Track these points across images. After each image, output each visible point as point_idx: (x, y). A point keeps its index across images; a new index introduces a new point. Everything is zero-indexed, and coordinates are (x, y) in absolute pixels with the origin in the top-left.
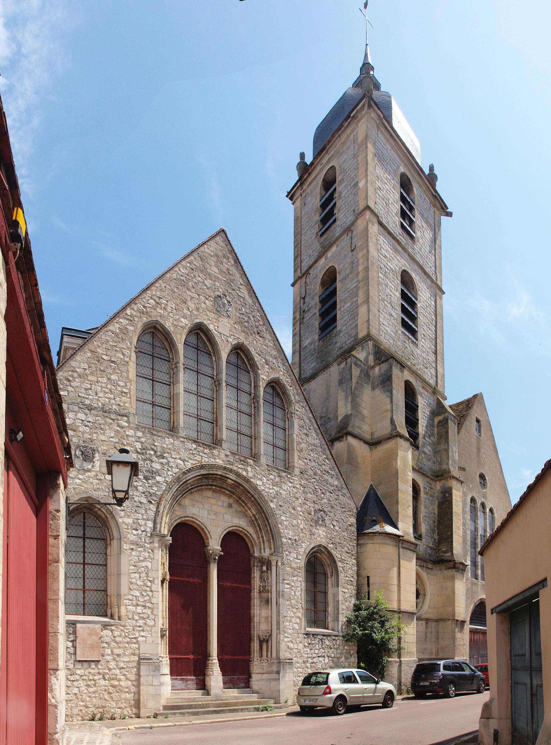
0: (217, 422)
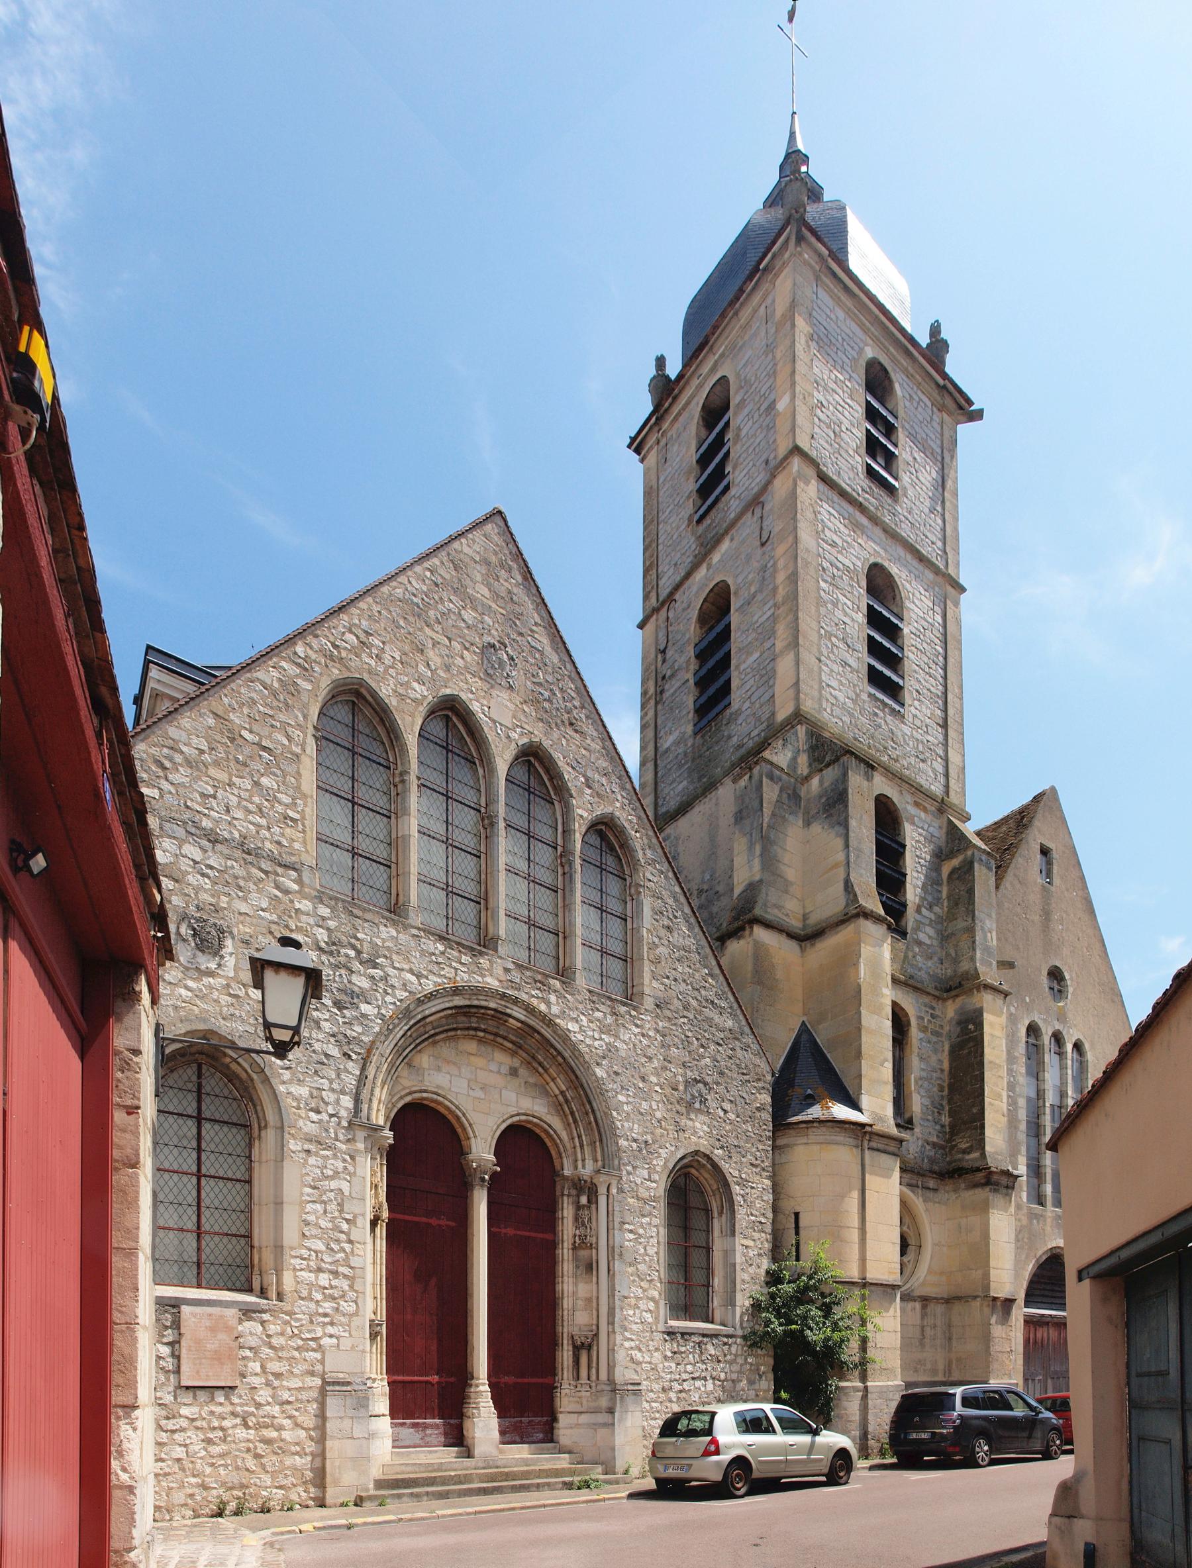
0: (486, 900)
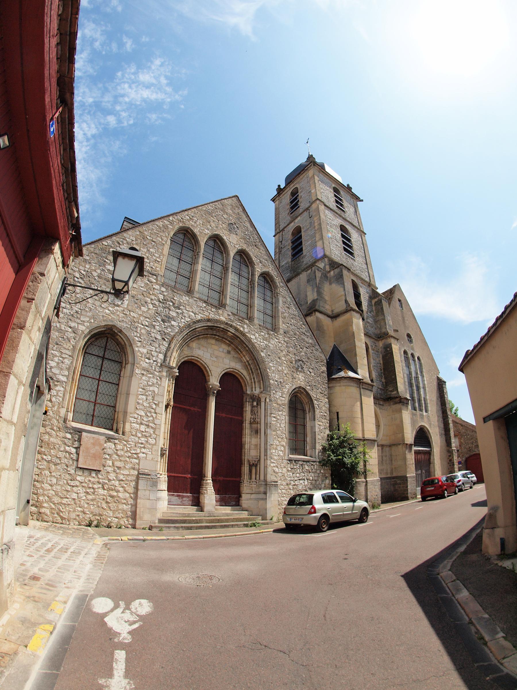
0: (223, 292)
